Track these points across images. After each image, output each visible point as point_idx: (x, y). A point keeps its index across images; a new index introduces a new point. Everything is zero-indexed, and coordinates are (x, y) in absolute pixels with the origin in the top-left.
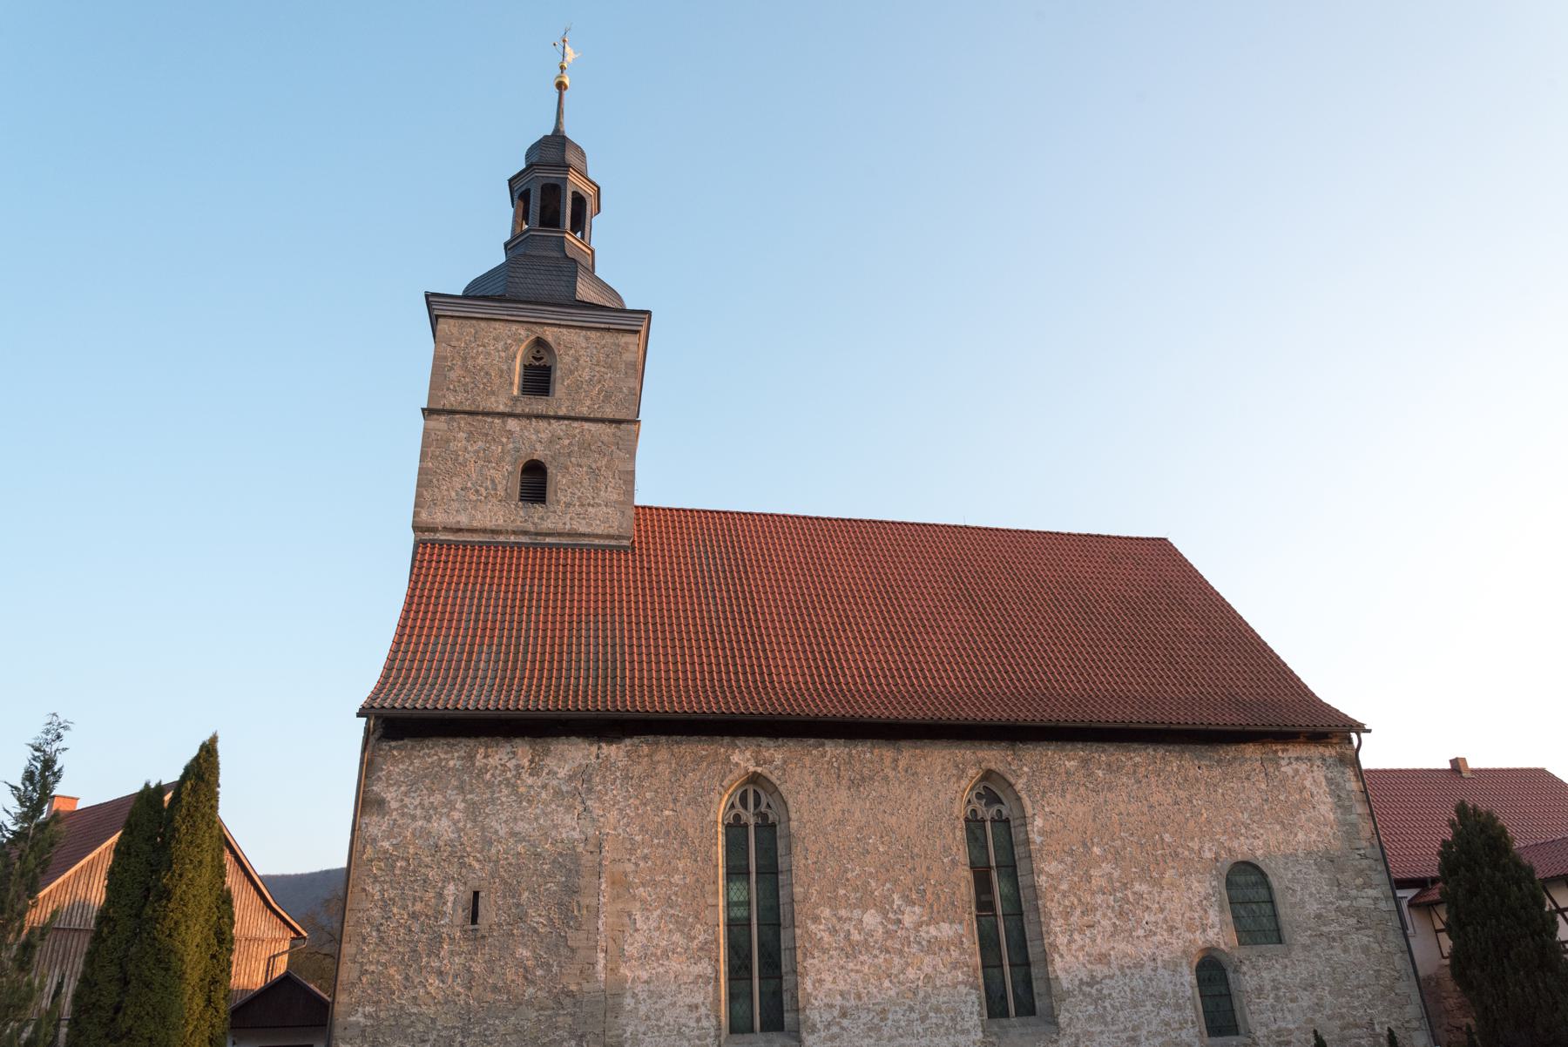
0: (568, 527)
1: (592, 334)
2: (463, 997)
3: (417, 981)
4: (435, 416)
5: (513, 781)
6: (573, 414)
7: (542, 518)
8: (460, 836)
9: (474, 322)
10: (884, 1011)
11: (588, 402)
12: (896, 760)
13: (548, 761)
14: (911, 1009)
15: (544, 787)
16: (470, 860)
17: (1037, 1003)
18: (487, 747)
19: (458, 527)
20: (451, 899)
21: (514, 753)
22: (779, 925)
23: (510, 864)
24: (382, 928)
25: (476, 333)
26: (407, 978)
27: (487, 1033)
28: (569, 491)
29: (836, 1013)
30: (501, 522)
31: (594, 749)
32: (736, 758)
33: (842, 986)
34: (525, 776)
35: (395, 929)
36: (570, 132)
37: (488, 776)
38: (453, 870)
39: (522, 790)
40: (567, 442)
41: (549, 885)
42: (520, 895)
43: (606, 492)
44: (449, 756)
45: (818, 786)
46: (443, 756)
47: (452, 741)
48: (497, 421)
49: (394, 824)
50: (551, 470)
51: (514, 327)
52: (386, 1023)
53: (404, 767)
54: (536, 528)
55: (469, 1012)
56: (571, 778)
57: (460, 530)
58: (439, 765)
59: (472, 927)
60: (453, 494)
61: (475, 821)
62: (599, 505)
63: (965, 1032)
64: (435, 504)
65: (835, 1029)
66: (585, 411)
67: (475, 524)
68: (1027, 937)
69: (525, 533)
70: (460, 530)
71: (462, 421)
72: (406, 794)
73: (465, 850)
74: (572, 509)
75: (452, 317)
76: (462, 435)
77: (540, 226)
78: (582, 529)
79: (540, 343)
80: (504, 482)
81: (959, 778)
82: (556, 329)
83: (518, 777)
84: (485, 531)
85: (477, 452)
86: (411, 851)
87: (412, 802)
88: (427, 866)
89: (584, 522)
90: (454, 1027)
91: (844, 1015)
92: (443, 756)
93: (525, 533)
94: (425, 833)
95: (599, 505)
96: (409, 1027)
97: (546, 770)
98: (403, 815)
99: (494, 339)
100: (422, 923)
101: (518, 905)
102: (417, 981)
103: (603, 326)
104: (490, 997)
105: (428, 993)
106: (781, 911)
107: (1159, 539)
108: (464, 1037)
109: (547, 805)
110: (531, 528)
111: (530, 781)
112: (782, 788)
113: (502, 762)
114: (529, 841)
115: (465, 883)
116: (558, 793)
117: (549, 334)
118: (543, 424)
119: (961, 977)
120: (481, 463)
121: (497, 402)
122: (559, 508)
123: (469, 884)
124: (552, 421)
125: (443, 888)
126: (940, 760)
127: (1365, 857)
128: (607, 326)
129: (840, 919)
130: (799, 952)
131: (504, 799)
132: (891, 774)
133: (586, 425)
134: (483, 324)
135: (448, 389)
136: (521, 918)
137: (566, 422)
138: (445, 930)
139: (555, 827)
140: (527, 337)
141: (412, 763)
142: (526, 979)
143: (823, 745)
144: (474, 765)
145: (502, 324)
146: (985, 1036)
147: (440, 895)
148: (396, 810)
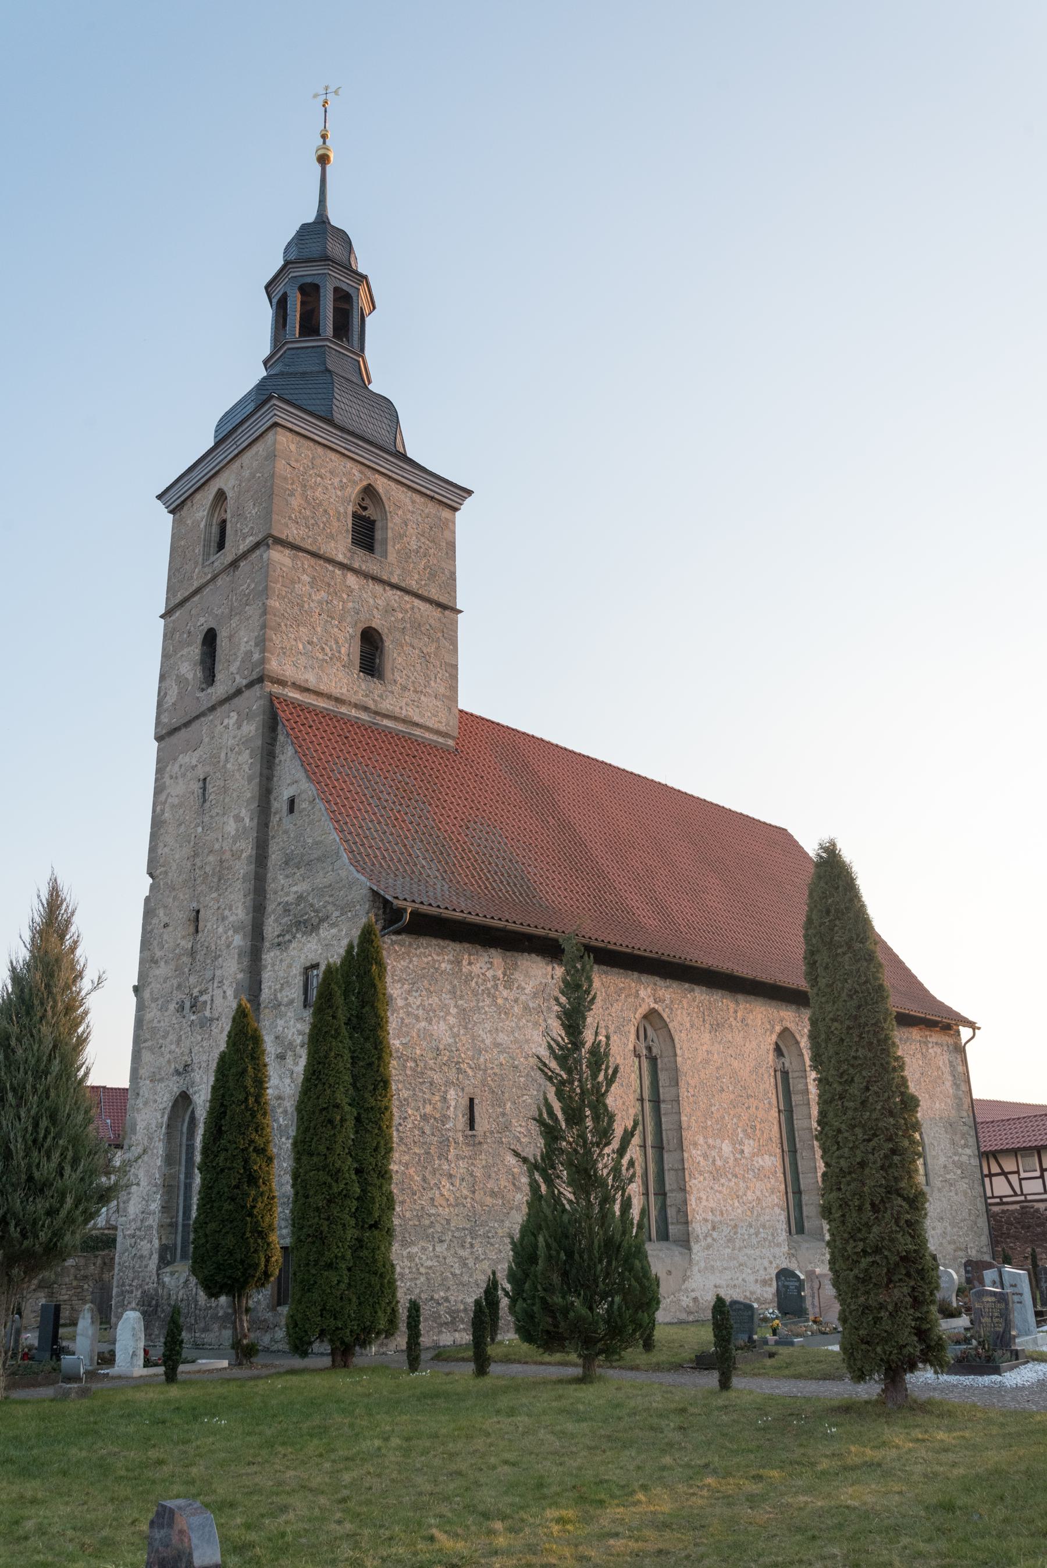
0: (404, 712)
1: (417, 498)
2: (469, 1200)
3: (432, 1182)
4: (280, 548)
5: (492, 991)
6: (403, 585)
7: (381, 696)
8: (456, 1043)
9: (311, 444)
10: (736, 1226)
11: (416, 577)
12: (736, 1012)
13: (517, 975)
14: (750, 1226)
15: (516, 1001)
16: (464, 1066)
17: (806, 1224)
18: (470, 955)
19: (306, 686)
20: (453, 1103)
21: (491, 963)
22: (663, 1148)
23: (495, 1074)
24: (401, 1128)
25: (313, 458)
26: (424, 1179)
27: (490, 1235)
28: (405, 672)
29: (710, 1227)
30: (344, 691)
31: (550, 968)
32: (642, 993)
33: (712, 1204)
34: (501, 988)
35: (411, 1130)
36: (336, 219)
37: (473, 984)
38: (452, 1075)
39: (500, 1001)
40: (400, 616)
41: (525, 1097)
42: (505, 1105)
43: (435, 682)
44: (440, 958)
45: (692, 1027)
46: (436, 957)
47: (442, 943)
48: (338, 572)
49: (402, 1023)
50: (388, 644)
51: (349, 464)
52: (411, 1223)
53: (405, 964)
54: (376, 706)
55: (475, 1214)
56: (535, 996)
57: (307, 690)
58: (433, 967)
59: (470, 1133)
60: (301, 646)
61: (466, 1028)
62: (430, 695)
63: (779, 1245)
64: (284, 653)
65: (709, 1240)
66: (414, 585)
67: (323, 688)
68: (800, 1170)
69: (366, 709)
70: (307, 690)
71: (307, 561)
72: (409, 992)
73: (460, 1057)
74: (407, 694)
75: (291, 430)
76: (306, 578)
77: (334, 337)
78: (416, 719)
79: (369, 491)
80: (347, 645)
81: (772, 1033)
82: (385, 481)
83: (496, 987)
84: (329, 697)
85: (320, 602)
86: (418, 1052)
87: (415, 1001)
88: (431, 1069)
89: (417, 710)
90: (464, 1229)
91: (714, 1228)
92: (436, 957)
93: (366, 709)
94: (427, 1035)
95: (430, 695)
96: (430, 1227)
97: (516, 985)
98: (408, 1014)
99: (331, 473)
100: (433, 1125)
101: (504, 1114)
102: (432, 1182)
103: (428, 492)
104: (489, 1200)
105: (443, 1195)
106: (664, 1138)
107: (780, 828)
108: (472, 1238)
109: (519, 1020)
110: (371, 705)
111: (505, 993)
112: (671, 1026)
113: (483, 971)
114: (508, 1053)
115: (463, 1089)
116: (526, 1008)
117: (381, 485)
118: (378, 588)
119: (776, 1201)
120: (324, 616)
121: (336, 548)
122: (396, 689)
123: (466, 1089)
124: (387, 588)
125: (446, 1092)
126: (760, 1016)
127: (965, 1124)
128: (432, 494)
129: (709, 1146)
130: (686, 1172)
131: (487, 1009)
132: (734, 1023)
133: (417, 602)
134: (320, 450)
135: (290, 518)
136: (507, 1127)
137: (399, 593)
138: (451, 1134)
139: (527, 1041)
140: (361, 480)
141: (411, 961)
142: (514, 1185)
143: (693, 990)
144: (461, 970)
145: (338, 456)
146: (790, 1249)
147: (444, 1099)
148: (402, 1008)
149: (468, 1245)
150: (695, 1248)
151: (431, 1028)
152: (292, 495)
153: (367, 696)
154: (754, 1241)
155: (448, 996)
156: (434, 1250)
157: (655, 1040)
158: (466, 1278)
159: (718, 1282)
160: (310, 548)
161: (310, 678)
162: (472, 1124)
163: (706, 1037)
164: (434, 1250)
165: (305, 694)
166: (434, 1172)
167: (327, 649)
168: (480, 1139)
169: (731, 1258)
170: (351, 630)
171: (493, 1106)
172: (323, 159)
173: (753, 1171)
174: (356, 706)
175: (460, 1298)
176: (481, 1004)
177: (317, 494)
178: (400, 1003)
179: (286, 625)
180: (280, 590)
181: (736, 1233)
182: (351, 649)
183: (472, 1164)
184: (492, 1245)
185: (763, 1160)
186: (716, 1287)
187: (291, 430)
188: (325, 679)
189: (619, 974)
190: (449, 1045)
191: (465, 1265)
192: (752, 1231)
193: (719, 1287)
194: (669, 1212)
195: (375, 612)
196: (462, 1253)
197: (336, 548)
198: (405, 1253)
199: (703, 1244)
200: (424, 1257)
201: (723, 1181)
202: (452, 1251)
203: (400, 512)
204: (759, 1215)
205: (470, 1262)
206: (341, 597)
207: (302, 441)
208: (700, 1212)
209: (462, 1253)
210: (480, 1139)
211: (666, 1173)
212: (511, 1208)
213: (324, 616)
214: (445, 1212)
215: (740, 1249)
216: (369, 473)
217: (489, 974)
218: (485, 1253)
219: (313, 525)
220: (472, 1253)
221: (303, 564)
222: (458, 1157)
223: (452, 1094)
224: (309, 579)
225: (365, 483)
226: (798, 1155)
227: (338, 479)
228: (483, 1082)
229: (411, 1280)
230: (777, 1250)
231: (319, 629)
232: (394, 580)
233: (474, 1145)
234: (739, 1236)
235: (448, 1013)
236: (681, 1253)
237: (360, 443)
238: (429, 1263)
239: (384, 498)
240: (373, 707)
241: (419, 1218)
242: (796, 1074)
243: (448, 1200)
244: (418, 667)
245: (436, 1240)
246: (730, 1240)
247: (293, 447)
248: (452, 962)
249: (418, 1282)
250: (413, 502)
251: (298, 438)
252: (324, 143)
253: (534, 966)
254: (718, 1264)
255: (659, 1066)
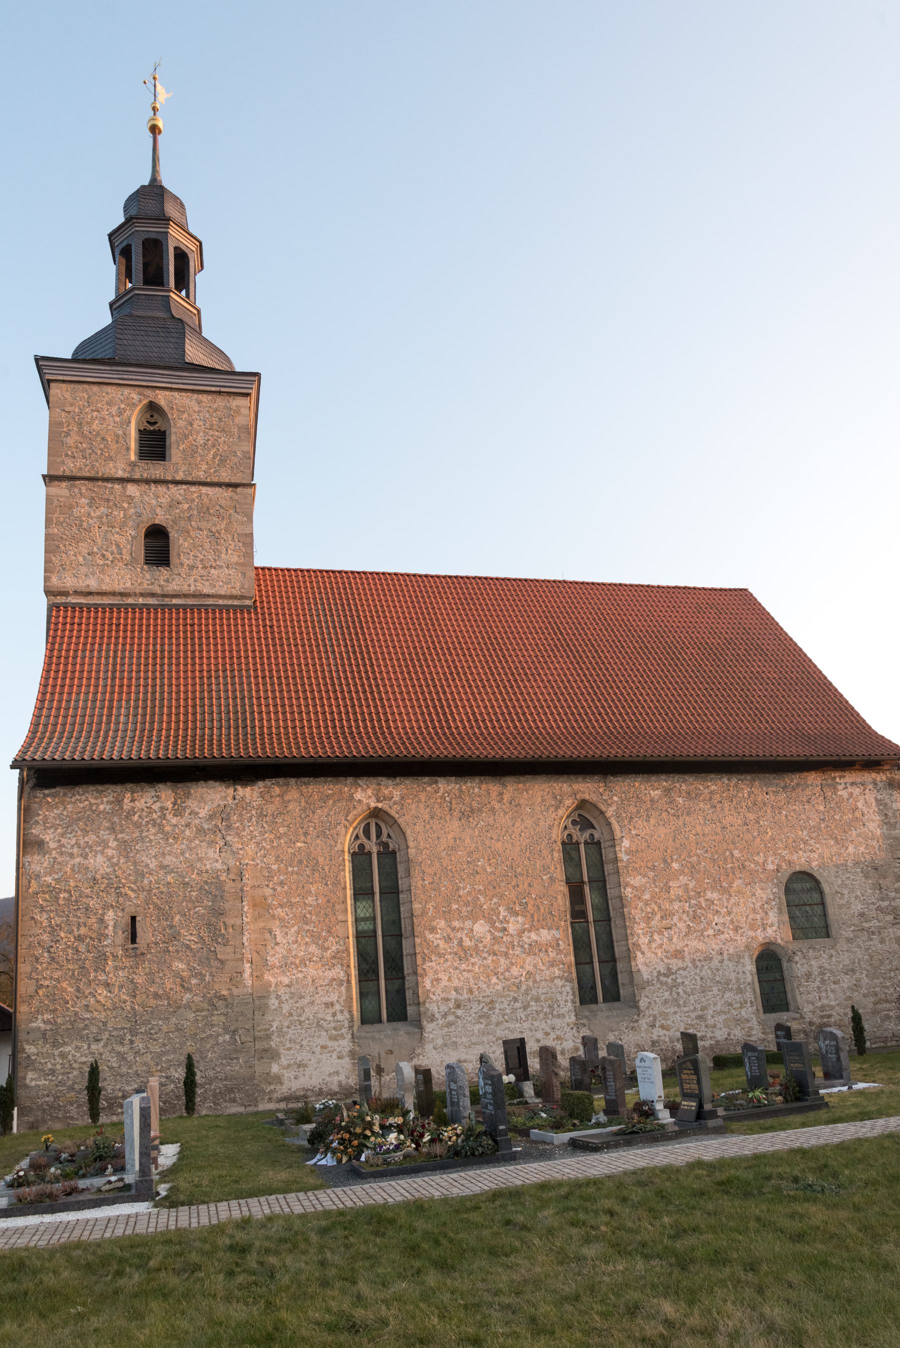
0: (192, 588)
1: (204, 398)
2: (128, 1003)
3: (87, 992)
4: (56, 483)
5: (159, 821)
7: (167, 581)
9: (86, 386)
11: (204, 467)
13: (189, 803)
14: (515, 1000)
15: (188, 825)
16: (126, 890)
17: (621, 991)
18: (133, 793)
19: (88, 590)
20: (111, 923)
21: (158, 797)
22: (401, 936)
23: (162, 893)
24: (52, 950)
25: (89, 397)
30: (128, 585)
34: (169, 817)
35: (63, 950)
37: (136, 818)
38: (111, 899)
39: (167, 829)
40: (186, 506)
41: (197, 909)
42: (172, 918)
44: (99, 801)
45: (432, 818)
46: (93, 801)
47: (100, 788)
48: (116, 486)
49: (54, 862)
51: (126, 391)
52: (64, 1027)
53: (59, 812)
54: (163, 590)
55: (135, 1015)
56: (211, 817)
59: (132, 946)
60: (81, 559)
62: (221, 567)
64: (64, 569)
65: (451, 1018)
66: (201, 475)
67: (104, 588)
69: (153, 595)
70: (90, 594)
71: (83, 486)
75: (64, 381)
76: (84, 501)
79: (153, 408)
80: (129, 546)
81: (557, 808)
82: (167, 393)
83: (163, 817)
84: (114, 594)
85: (100, 517)
87: (69, 842)
88: (87, 896)
89: (207, 583)
90: (123, 1028)
92: (93, 801)
93: (153, 595)
95: (221, 567)
96: (84, 1029)
97: (188, 811)
98: (62, 854)
101: (171, 927)
102: (87, 992)
103: (213, 389)
104: (153, 1002)
105: (98, 1002)
109: (191, 842)
111: (174, 821)
114: (177, 872)
115: (123, 910)
116: (200, 830)
117: (162, 398)
118: (162, 489)
120: (105, 528)
121: (115, 467)
123: (127, 910)
124: (170, 486)
125: (103, 915)
126: (540, 793)
128: (217, 389)
131: (152, 837)
133: (204, 489)
134: (95, 388)
135: (66, 455)
136: (175, 937)
137: (184, 487)
138: (108, 949)
140: (140, 401)
141: (65, 808)
143: (436, 782)
144: (122, 808)
145: (114, 387)
147: (101, 921)
148: (55, 849)
149: (126, 1042)
150: (429, 1027)
151: (86, 862)
152: (68, 434)
153: (152, 583)
154: (521, 1014)
155: (107, 832)
156: (89, 1048)
157: (392, 834)
158: (124, 1070)
160: (88, 475)
161: (93, 584)
162: (134, 938)
163: (456, 824)
164: (89, 1048)
166: (90, 983)
167: (108, 555)
170: (133, 533)
171: (159, 920)
172: (154, 130)
174: (142, 595)
175: (118, 1087)
176: (145, 834)
177: (94, 427)
179: (65, 546)
180: (57, 518)
182: (179, 543)
183: (134, 972)
184: (155, 1040)
187: (64, 381)
188: (107, 580)
189: (325, 782)
190: (108, 874)
191: (124, 1059)
194: (407, 994)
195: (158, 510)
196: (120, 1049)
197: (115, 467)
198: (56, 1053)
200: (78, 1055)
202: (109, 1048)
203: (185, 416)
205: (130, 1057)
206: (122, 507)
207: (77, 386)
209: (120, 1049)
211: (405, 958)
213: (105, 528)
214: (102, 1016)
216: (149, 392)
217: (156, 807)
219: (90, 454)
221: (80, 489)
222: (116, 968)
223: (110, 915)
224: (87, 501)
225: (145, 402)
226: (613, 924)
227: (116, 408)
228: (147, 902)
229: (63, 1074)
230: (558, 1022)
231: (99, 541)
232: (180, 476)
233: (136, 956)
236: (408, 1033)
237: (131, 369)
239: (166, 408)
240: (159, 592)
242: (608, 843)
243: (104, 1005)
244: (207, 546)
245: (91, 1039)
247: (68, 395)
248: (111, 803)
249: (70, 1076)
250: (199, 402)
251: (72, 386)
252: (155, 114)
253: (211, 791)
255: (398, 860)
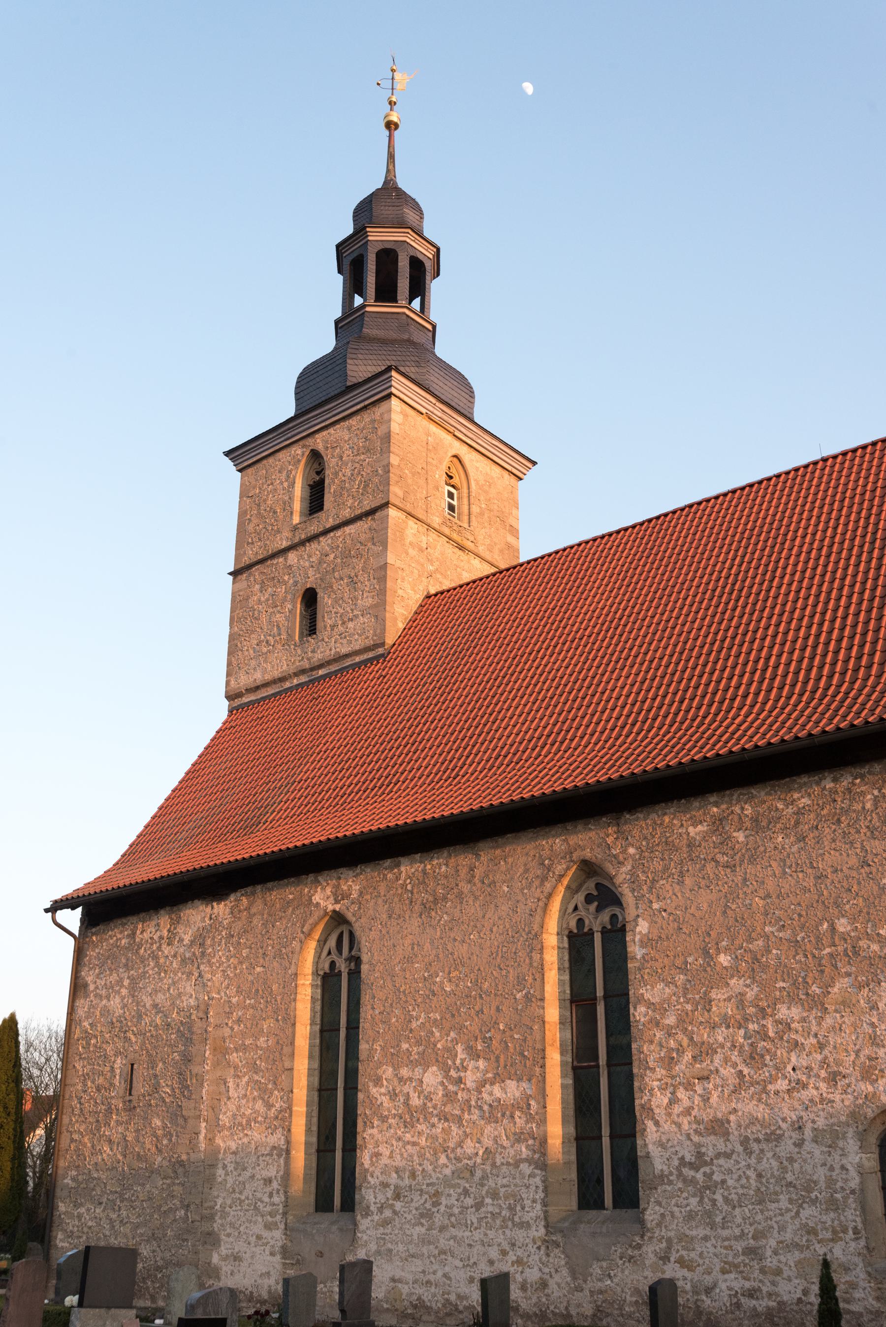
10: (437, 1194)
14: (466, 1192)
29: (390, 1194)
30: (285, 667)
33: (398, 1162)
57: (257, 688)
65: (388, 1213)
70: (257, 688)
78: (345, 650)
91: (397, 1196)
103: (358, 407)
126: (523, 860)
128: (362, 405)
129: (401, 1080)
133: (348, 529)
143: (398, 865)
149: (116, 1208)
154: (472, 1217)
159: (398, 1274)
165: (259, 691)
168: (135, 1103)
169: (424, 1241)
173: (480, 1108)
174: (296, 674)
178: (92, 987)
181: (436, 1204)
185: (504, 1089)
186: (393, 1280)
192: (469, 1201)
193: (400, 1281)
199: (376, 1218)
200: (88, 1217)
201: (420, 1127)
204: (484, 1177)
208: (377, 1173)
210: (135, 1103)
212: (152, 1172)
215: (442, 1229)
218: (128, 1217)
220: (119, 1216)
230: (520, 1235)
234: (442, 1208)
235: (122, 986)
238: (90, 1224)
241: (87, 1181)
246: (427, 1215)
254: (401, 1247)
